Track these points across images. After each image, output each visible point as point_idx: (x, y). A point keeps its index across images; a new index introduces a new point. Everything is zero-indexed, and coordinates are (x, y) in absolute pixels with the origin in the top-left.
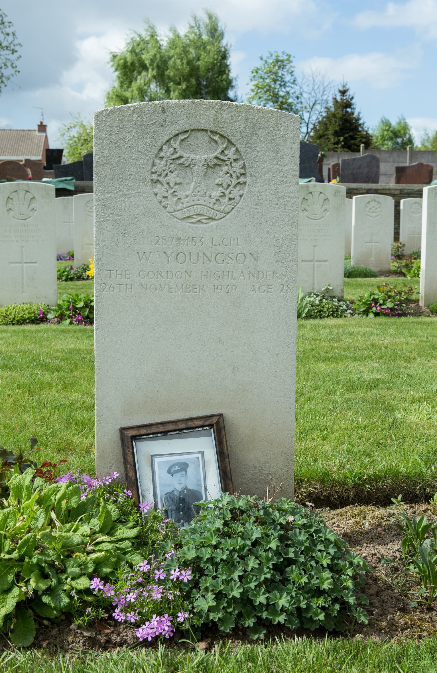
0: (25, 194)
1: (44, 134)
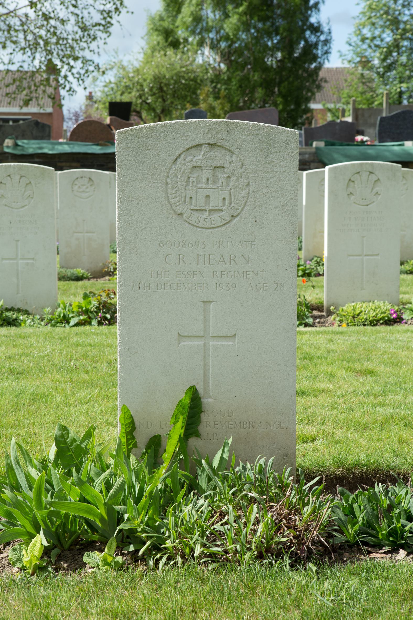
0: (369, 175)
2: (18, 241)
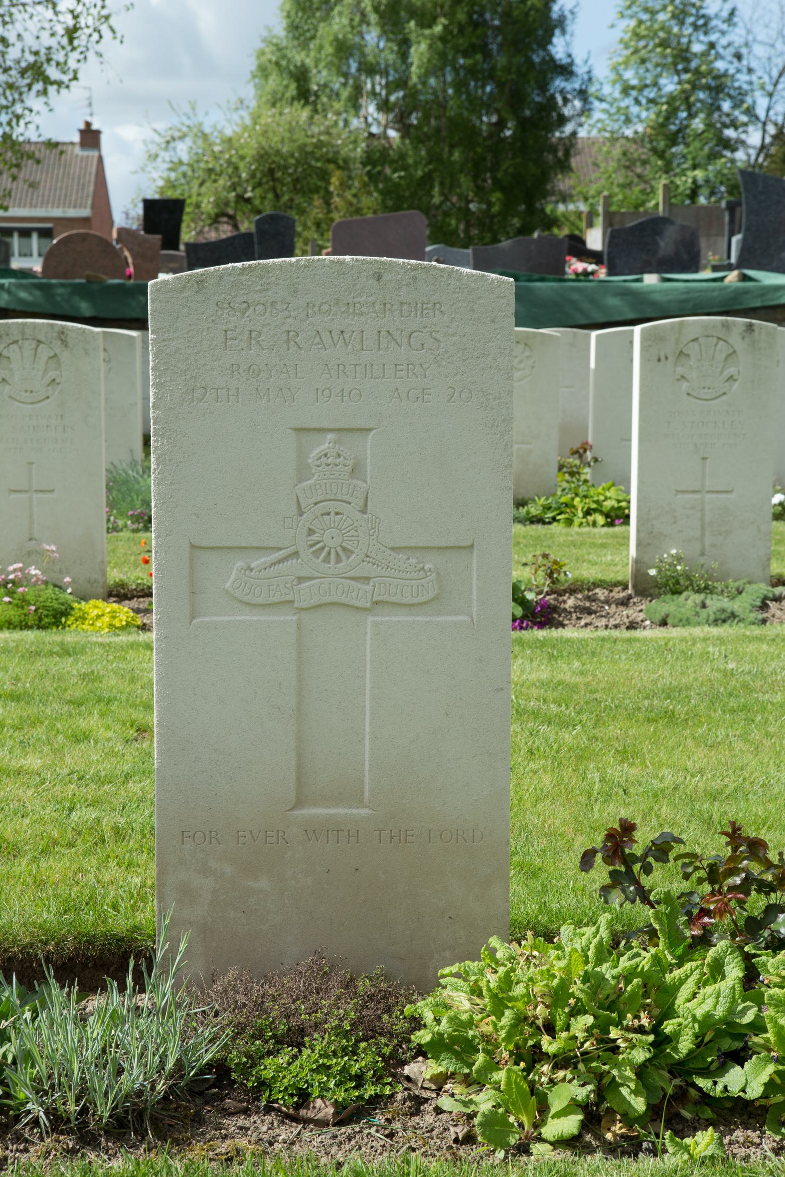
1: (96, 154)
2: (32, 463)
